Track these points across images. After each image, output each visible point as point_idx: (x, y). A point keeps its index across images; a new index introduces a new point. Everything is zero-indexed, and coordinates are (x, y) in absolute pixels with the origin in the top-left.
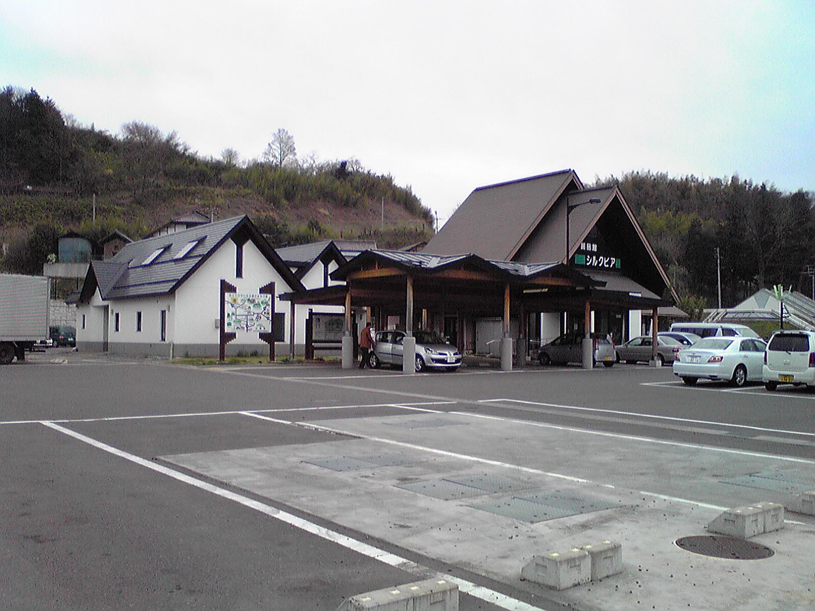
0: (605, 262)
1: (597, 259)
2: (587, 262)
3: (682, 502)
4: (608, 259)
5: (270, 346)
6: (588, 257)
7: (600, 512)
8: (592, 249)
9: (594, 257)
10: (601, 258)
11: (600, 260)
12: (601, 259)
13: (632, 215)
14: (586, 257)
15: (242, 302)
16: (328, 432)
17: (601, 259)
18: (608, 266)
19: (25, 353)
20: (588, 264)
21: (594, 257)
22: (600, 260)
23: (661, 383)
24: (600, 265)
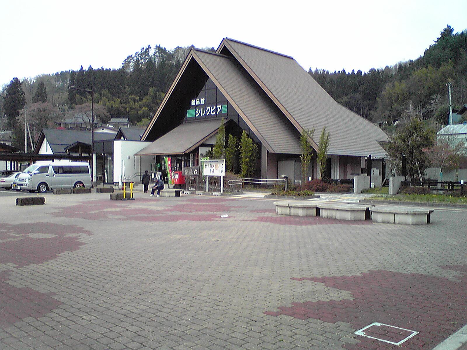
0: (212, 110)
1: (205, 109)
2: (196, 114)
3: (125, 166)
4: (215, 107)
5: (262, 198)
6: (197, 110)
7: (407, 338)
8: (200, 103)
9: (202, 109)
10: (208, 108)
11: (207, 110)
12: (209, 109)
13: (148, 128)
14: (196, 110)
15: (59, 81)
16: (46, 98)
17: (209, 109)
18: (214, 113)
19: (9, 163)
20: (197, 116)
21: (202, 109)
22: (207, 110)
23: (320, 202)
24: (207, 114)
